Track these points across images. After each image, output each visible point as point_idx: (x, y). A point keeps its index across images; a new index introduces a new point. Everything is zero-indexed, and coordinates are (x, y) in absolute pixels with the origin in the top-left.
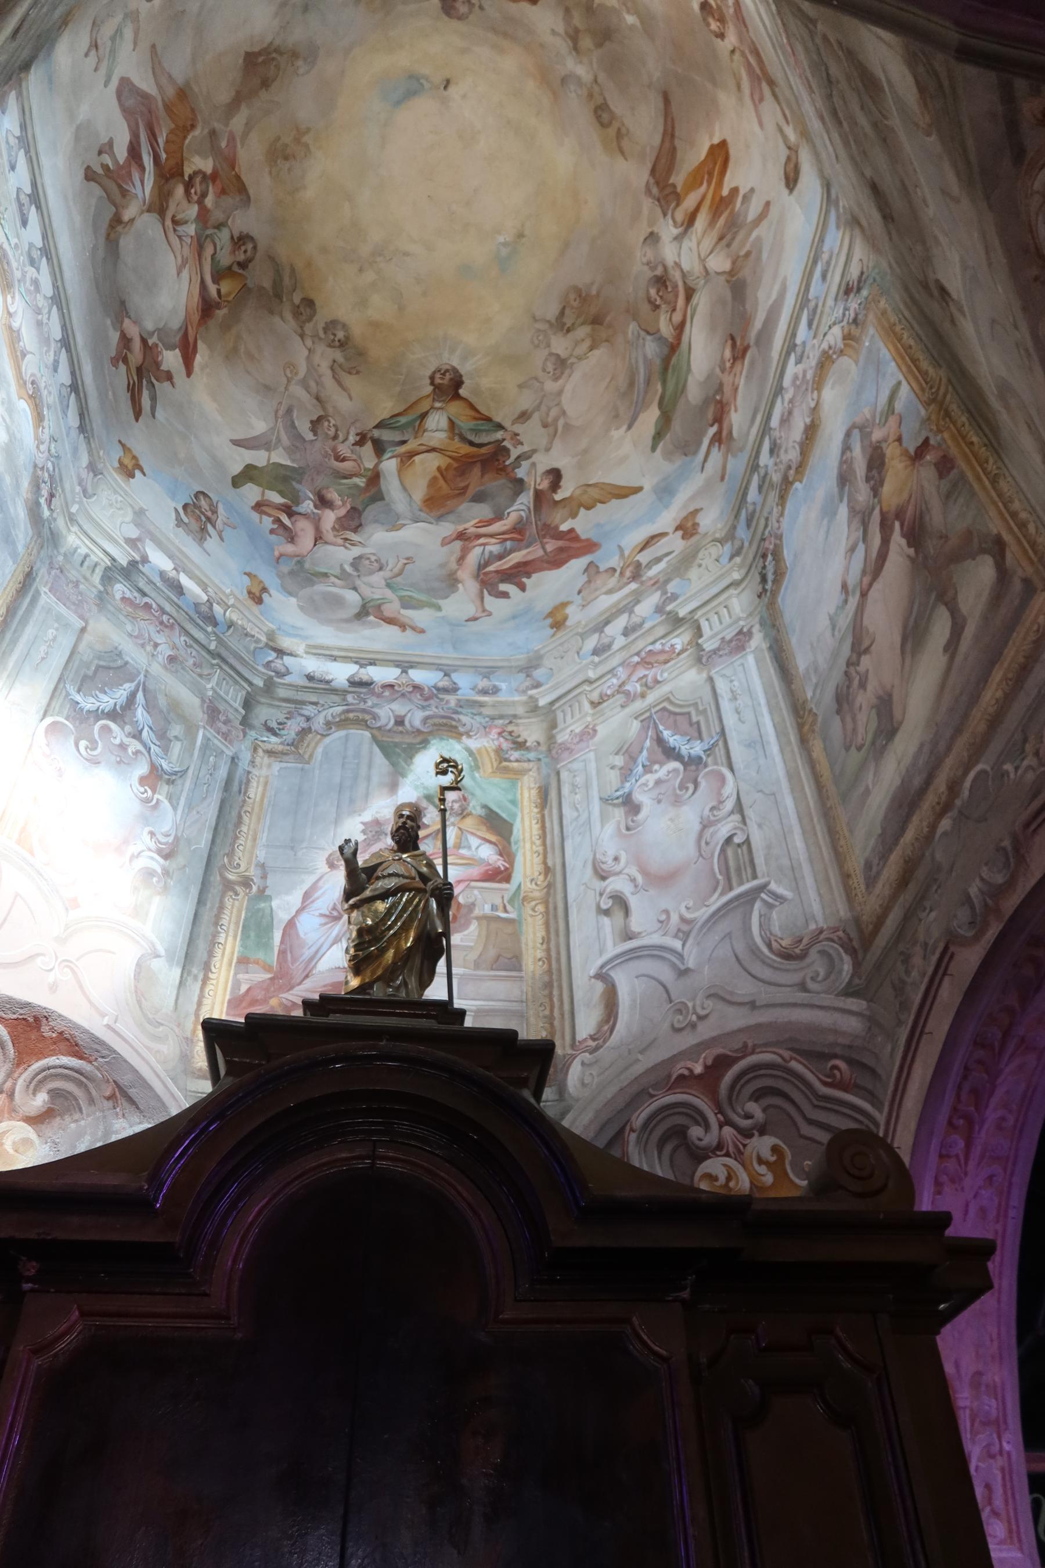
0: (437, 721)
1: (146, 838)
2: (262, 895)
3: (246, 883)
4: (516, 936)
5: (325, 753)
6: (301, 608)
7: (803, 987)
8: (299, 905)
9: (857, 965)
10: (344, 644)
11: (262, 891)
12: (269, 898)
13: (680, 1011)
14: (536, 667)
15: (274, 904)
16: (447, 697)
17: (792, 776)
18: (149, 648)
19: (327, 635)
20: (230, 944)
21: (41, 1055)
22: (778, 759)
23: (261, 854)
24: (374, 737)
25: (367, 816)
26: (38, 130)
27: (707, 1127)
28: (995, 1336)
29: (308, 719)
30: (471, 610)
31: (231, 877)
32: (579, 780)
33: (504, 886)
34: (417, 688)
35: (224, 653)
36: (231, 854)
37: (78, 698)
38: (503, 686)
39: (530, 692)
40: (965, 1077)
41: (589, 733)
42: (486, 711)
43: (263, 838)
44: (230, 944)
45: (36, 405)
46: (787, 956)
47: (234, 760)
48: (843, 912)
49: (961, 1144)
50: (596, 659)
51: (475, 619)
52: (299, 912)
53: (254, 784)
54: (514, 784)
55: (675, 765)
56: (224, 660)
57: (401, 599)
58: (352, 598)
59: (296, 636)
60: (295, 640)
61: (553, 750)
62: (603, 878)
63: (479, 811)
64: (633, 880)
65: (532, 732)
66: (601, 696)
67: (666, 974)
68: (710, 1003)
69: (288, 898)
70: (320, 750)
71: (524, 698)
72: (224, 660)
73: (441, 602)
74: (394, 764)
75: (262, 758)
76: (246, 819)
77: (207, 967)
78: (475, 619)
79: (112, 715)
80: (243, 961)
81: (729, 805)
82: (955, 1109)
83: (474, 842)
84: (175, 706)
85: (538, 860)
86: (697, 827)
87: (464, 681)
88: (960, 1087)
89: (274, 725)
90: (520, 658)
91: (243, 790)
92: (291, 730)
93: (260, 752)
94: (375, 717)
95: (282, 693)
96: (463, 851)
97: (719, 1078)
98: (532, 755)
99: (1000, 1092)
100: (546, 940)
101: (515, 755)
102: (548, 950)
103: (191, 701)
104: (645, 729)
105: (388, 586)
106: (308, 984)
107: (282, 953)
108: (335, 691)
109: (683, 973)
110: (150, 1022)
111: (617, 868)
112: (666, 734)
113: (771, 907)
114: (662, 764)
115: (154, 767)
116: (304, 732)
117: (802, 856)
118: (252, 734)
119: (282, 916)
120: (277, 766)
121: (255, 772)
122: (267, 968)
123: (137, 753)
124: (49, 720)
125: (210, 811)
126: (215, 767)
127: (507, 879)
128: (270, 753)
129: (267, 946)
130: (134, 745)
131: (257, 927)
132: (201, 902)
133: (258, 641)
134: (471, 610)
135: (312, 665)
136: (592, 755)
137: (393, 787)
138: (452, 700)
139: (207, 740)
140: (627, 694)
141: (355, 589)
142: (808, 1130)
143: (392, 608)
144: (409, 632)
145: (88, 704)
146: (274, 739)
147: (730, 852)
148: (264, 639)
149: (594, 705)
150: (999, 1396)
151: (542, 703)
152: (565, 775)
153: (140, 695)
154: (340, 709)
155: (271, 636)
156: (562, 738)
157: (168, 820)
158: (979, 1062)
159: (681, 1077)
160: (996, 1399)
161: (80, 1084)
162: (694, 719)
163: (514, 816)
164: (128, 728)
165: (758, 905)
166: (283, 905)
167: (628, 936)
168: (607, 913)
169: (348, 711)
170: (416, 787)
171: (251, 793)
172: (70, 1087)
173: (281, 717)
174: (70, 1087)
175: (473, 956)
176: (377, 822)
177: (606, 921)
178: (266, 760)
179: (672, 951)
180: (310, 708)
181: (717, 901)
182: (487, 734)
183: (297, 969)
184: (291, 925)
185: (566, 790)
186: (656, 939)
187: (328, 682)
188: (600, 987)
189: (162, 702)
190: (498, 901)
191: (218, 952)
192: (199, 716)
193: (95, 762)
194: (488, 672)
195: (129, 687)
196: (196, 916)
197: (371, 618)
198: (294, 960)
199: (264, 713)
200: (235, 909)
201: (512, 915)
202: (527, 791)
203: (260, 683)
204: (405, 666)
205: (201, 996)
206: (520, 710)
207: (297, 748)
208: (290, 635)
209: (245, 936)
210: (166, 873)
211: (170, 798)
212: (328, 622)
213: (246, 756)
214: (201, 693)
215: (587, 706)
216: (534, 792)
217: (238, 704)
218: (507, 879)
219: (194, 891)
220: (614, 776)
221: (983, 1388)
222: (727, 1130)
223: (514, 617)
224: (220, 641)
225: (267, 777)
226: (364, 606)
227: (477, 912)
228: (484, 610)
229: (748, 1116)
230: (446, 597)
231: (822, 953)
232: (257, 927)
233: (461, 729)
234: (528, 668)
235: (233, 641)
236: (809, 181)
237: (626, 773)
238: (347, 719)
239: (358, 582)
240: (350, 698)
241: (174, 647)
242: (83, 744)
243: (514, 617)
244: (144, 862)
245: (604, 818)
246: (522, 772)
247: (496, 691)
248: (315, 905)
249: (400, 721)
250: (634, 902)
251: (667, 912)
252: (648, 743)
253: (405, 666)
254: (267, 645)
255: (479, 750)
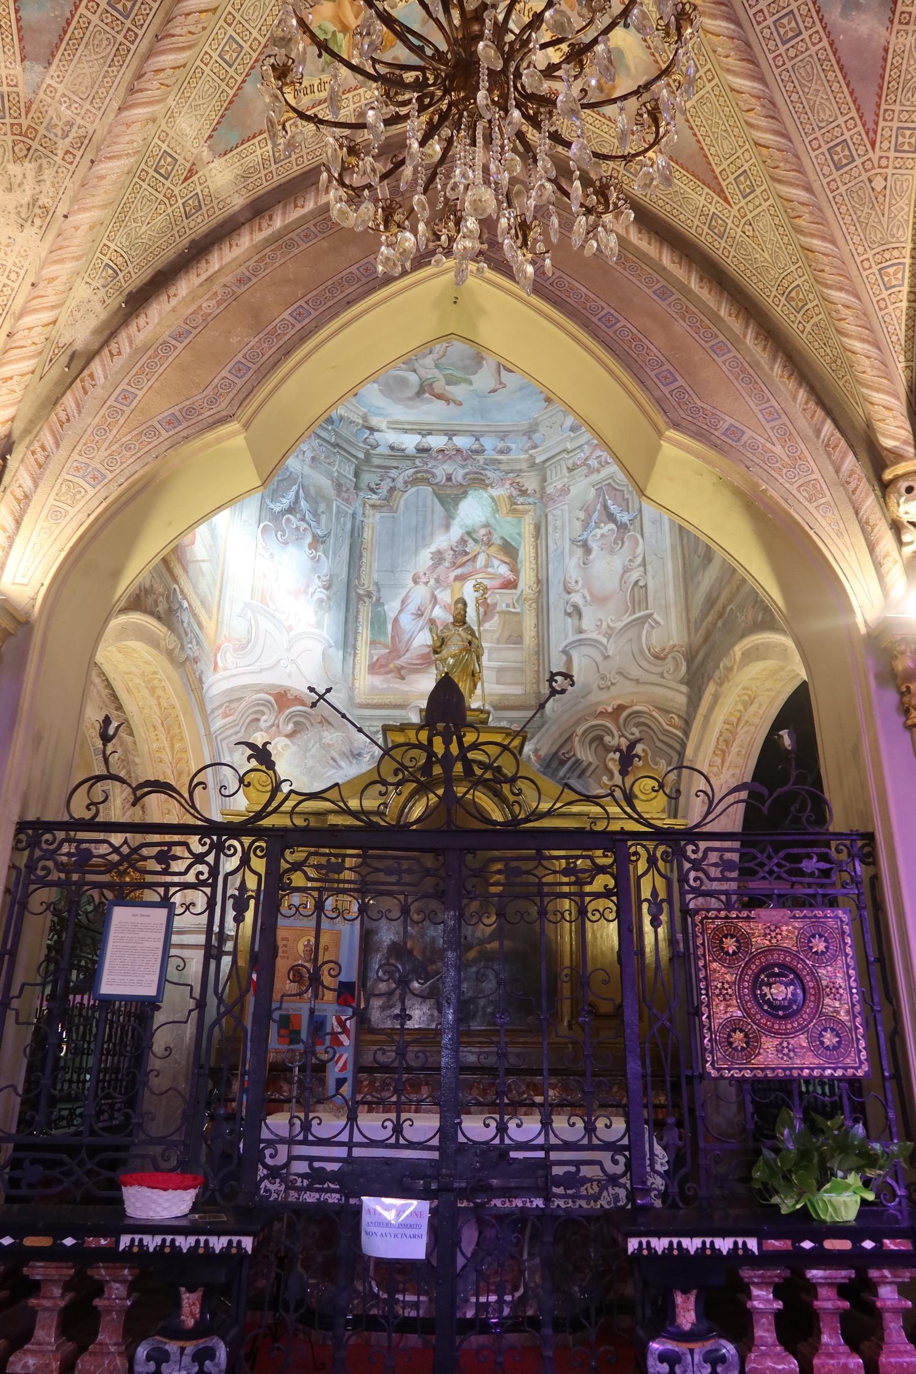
0: (472, 476)
1: (316, 580)
2: (379, 603)
3: (369, 595)
4: (520, 623)
5: (406, 504)
6: (381, 390)
7: (662, 675)
8: (399, 608)
9: (688, 668)
10: (411, 418)
11: (378, 600)
12: (382, 605)
13: (603, 679)
14: (535, 431)
15: (386, 608)
16: (478, 457)
17: (673, 548)
18: (301, 457)
19: (400, 413)
20: (365, 634)
21: (289, 707)
22: (668, 535)
23: (375, 576)
24: (434, 490)
25: (433, 548)
27: (613, 737)
29: (393, 480)
30: (492, 383)
31: (361, 592)
32: (559, 523)
33: (513, 591)
34: (459, 451)
35: (340, 442)
36: (359, 578)
37: (272, 506)
38: (513, 446)
39: (531, 452)
41: (565, 491)
42: (503, 467)
43: (375, 566)
44: (365, 634)
46: (657, 657)
47: (354, 515)
48: (686, 639)
50: (572, 435)
51: (494, 391)
52: (400, 612)
53: (366, 529)
54: (520, 520)
55: (612, 526)
56: (340, 447)
57: (445, 376)
58: (413, 378)
59: (380, 415)
60: (380, 418)
61: (544, 498)
62: (569, 593)
63: (499, 542)
64: (585, 597)
65: (531, 483)
66: (574, 464)
67: (598, 657)
68: (617, 676)
69: (393, 604)
70: (402, 502)
71: (527, 456)
72: (340, 447)
73: (472, 377)
74: (447, 510)
75: (369, 511)
76: (364, 553)
77: (355, 647)
78: (494, 391)
79: (291, 510)
80: (373, 643)
81: (639, 560)
83: (496, 563)
84: (319, 490)
85: (533, 574)
86: (621, 571)
87: (488, 443)
89: (373, 486)
90: (524, 424)
91: (360, 535)
92: (385, 486)
93: (368, 507)
94: (434, 476)
95: (376, 461)
96: (489, 570)
97: (619, 715)
98: (531, 500)
99: (737, 741)
100: (537, 626)
101: (521, 500)
102: (538, 632)
103: (326, 483)
104: (598, 496)
105: (436, 366)
106: (408, 655)
107: (393, 637)
108: (407, 457)
109: (606, 657)
111: (577, 588)
112: (609, 502)
113: (652, 627)
114: (606, 524)
115: (315, 537)
116: (392, 490)
117: (672, 601)
118: (361, 494)
119: (391, 615)
120: (378, 515)
121: (366, 520)
122: (387, 647)
123: (305, 529)
124: (262, 525)
125: (345, 553)
126: (344, 524)
127: (515, 587)
128: (373, 506)
129: (385, 633)
130: (303, 525)
131: (378, 622)
132: (347, 610)
133: (358, 424)
134: (492, 383)
135: (392, 437)
136: (566, 507)
137: (447, 527)
138: (480, 458)
139: (338, 507)
140: (589, 466)
141: (414, 371)
142: (659, 744)
143: (440, 386)
144: (452, 404)
145: (277, 507)
146: (374, 496)
147: (636, 590)
148: (361, 421)
149: (570, 470)
151: (538, 460)
152: (550, 517)
153: (301, 491)
154: (412, 471)
155: (365, 418)
156: (550, 490)
157: (326, 565)
159: (601, 713)
161: (306, 718)
162: (626, 496)
163: (520, 543)
164: (298, 516)
165: (646, 625)
166: (392, 608)
167: (581, 631)
168: (569, 615)
169: (417, 472)
170: (461, 526)
171: (365, 536)
172: (302, 719)
173: (377, 481)
174: (302, 719)
175: (496, 636)
176: (439, 552)
177: (569, 620)
178: (371, 512)
179: (602, 644)
180: (394, 471)
181: (627, 619)
182: (503, 484)
183: (402, 646)
184: (396, 620)
185: (550, 529)
186: (594, 635)
187: (403, 450)
188: (564, 658)
189: (312, 491)
190: (510, 602)
191: (359, 638)
192: (331, 492)
193: (286, 543)
194: (503, 435)
195: (295, 488)
196: (346, 619)
197: (427, 395)
198: (400, 641)
199: (368, 478)
200: (365, 612)
201: (518, 610)
202: (527, 527)
203: (361, 456)
204: (450, 434)
205: (354, 664)
206: (524, 466)
207: (388, 503)
208: (376, 415)
209: (372, 628)
210: (329, 598)
211: (324, 553)
212: (398, 401)
213: (360, 511)
214: (329, 475)
215: (565, 470)
216: (532, 526)
217: (351, 477)
218: (515, 587)
219: (343, 605)
220: (578, 525)
222: (623, 740)
223: (521, 389)
224: (337, 434)
225: (374, 522)
226: (421, 385)
227: (498, 609)
228: (501, 383)
229: (633, 734)
230: (475, 373)
231: (674, 658)
232: (378, 622)
233: (487, 482)
234: (529, 432)
235: (345, 432)
236: (573, 582)
237: (586, 525)
238: (417, 479)
239: (416, 365)
240: (417, 462)
241: (314, 450)
242: (279, 533)
243: (521, 389)
244: (318, 595)
245: (571, 554)
246: (525, 512)
247: (508, 451)
248: (409, 608)
249: (449, 479)
250: (585, 611)
251: (601, 620)
252: (599, 507)
253: (450, 434)
254: (363, 426)
255: (498, 497)
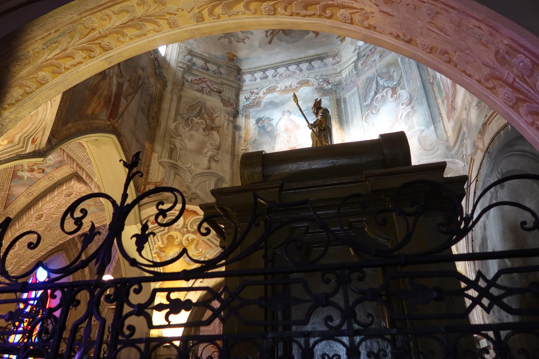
26: (253, 66)
28: (477, 24)
40: (298, 14)
45: (234, 147)
49: (342, 11)
82: (320, 16)
88: (305, 16)
110: (430, 150)
150: (519, 48)
158: (285, 9)
160: (520, 53)
221: (507, 57)
